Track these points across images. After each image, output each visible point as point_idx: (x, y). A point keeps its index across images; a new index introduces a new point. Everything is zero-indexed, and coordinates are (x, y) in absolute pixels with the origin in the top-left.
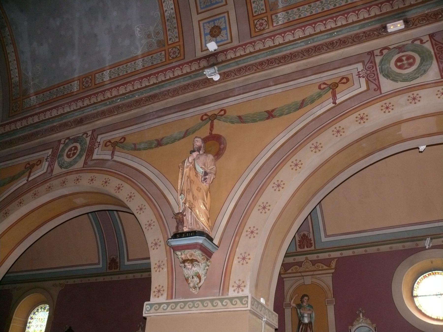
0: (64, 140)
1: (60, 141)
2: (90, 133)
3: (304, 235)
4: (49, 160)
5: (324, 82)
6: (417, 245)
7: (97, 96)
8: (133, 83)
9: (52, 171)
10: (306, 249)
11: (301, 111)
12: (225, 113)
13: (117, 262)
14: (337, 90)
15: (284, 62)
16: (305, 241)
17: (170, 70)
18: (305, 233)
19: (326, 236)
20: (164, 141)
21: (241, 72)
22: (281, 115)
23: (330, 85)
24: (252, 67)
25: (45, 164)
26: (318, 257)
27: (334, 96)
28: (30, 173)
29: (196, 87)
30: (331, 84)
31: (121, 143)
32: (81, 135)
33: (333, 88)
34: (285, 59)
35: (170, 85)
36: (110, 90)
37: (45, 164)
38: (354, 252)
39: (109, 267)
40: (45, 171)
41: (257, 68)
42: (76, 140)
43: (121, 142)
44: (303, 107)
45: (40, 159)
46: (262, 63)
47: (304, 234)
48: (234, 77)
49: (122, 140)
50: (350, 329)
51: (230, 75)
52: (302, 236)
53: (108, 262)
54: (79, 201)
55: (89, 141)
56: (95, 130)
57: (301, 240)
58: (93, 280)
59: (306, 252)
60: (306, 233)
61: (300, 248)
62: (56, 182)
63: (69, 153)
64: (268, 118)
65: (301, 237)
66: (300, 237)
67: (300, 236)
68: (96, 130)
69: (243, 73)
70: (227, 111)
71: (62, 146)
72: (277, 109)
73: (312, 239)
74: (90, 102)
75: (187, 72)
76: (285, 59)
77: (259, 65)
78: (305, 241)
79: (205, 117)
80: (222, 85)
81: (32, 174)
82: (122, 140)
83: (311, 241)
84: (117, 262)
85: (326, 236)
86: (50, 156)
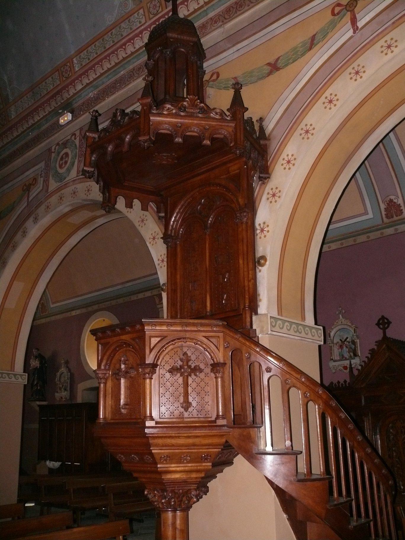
0: (55, 146)
1: (50, 150)
2: (78, 133)
3: (391, 201)
4: (43, 175)
5: (337, 2)
6: (396, 230)
7: (187, 5)
8: (124, 47)
9: (48, 186)
10: (395, 218)
11: (312, 51)
12: (218, 76)
13: (400, 204)
14: (356, 10)
15: (228, 17)
16: (393, 209)
17: (137, 37)
18: (392, 199)
19: (366, 213)
20: (280, 64)
21: (231, 13)
22: (287, 65)
23: (346, 6)
24: (244, 2)
25: (41, 180)
26: (382, 233)
27: (354, 21)
28: (29, 194)
29: (141, 72)
30: (347, 4)
31: (214, 81)
32: (69, 137)
33: (351, 9)
34: (229, 14)
35: (214, 10)
36: (108, 58)
37: (41, 180)
38: (368, 237)
39: (385, 215)
40: (41, 188)
41: (224, 18)
42: (65, 145)
43: (214, 80)
44: (313, 48)
45: (217, 71)
46: (230, 9)
47: (390, 199)
48: (249, 5)
49: (215, 77)
50: (329, 333)
51: (244, 4)
52: (388, 202)
53: (383, 206)
54: (76, 219)
55: (78, 144)
56: (82, 128)
57: (387, 207)
58: (141, 296)
59: (358, 233)
60: (392, 197)
61: (387, 218)
62: (54, 199)
63: (61, 162)
64: (270, 73)
65: (387, 203)
66: (386, 205)
67: (386, 203)
68: (83, 127)
69: (233, 13)
70: (220, 73)
71: (53, 155)
72: (281, 58)
73: (401, 205)
74: (126, 54)
75: (108, 68)
76: (229, 14)
77: (226, 12)
78: (393, 209)
79: (337, 10)
80: (261, 5)
81: (30, 194)
82: (215, 77)
83: (401, 206)
84: (400, 204)
85: (366, 213)
86: (44, 171)
